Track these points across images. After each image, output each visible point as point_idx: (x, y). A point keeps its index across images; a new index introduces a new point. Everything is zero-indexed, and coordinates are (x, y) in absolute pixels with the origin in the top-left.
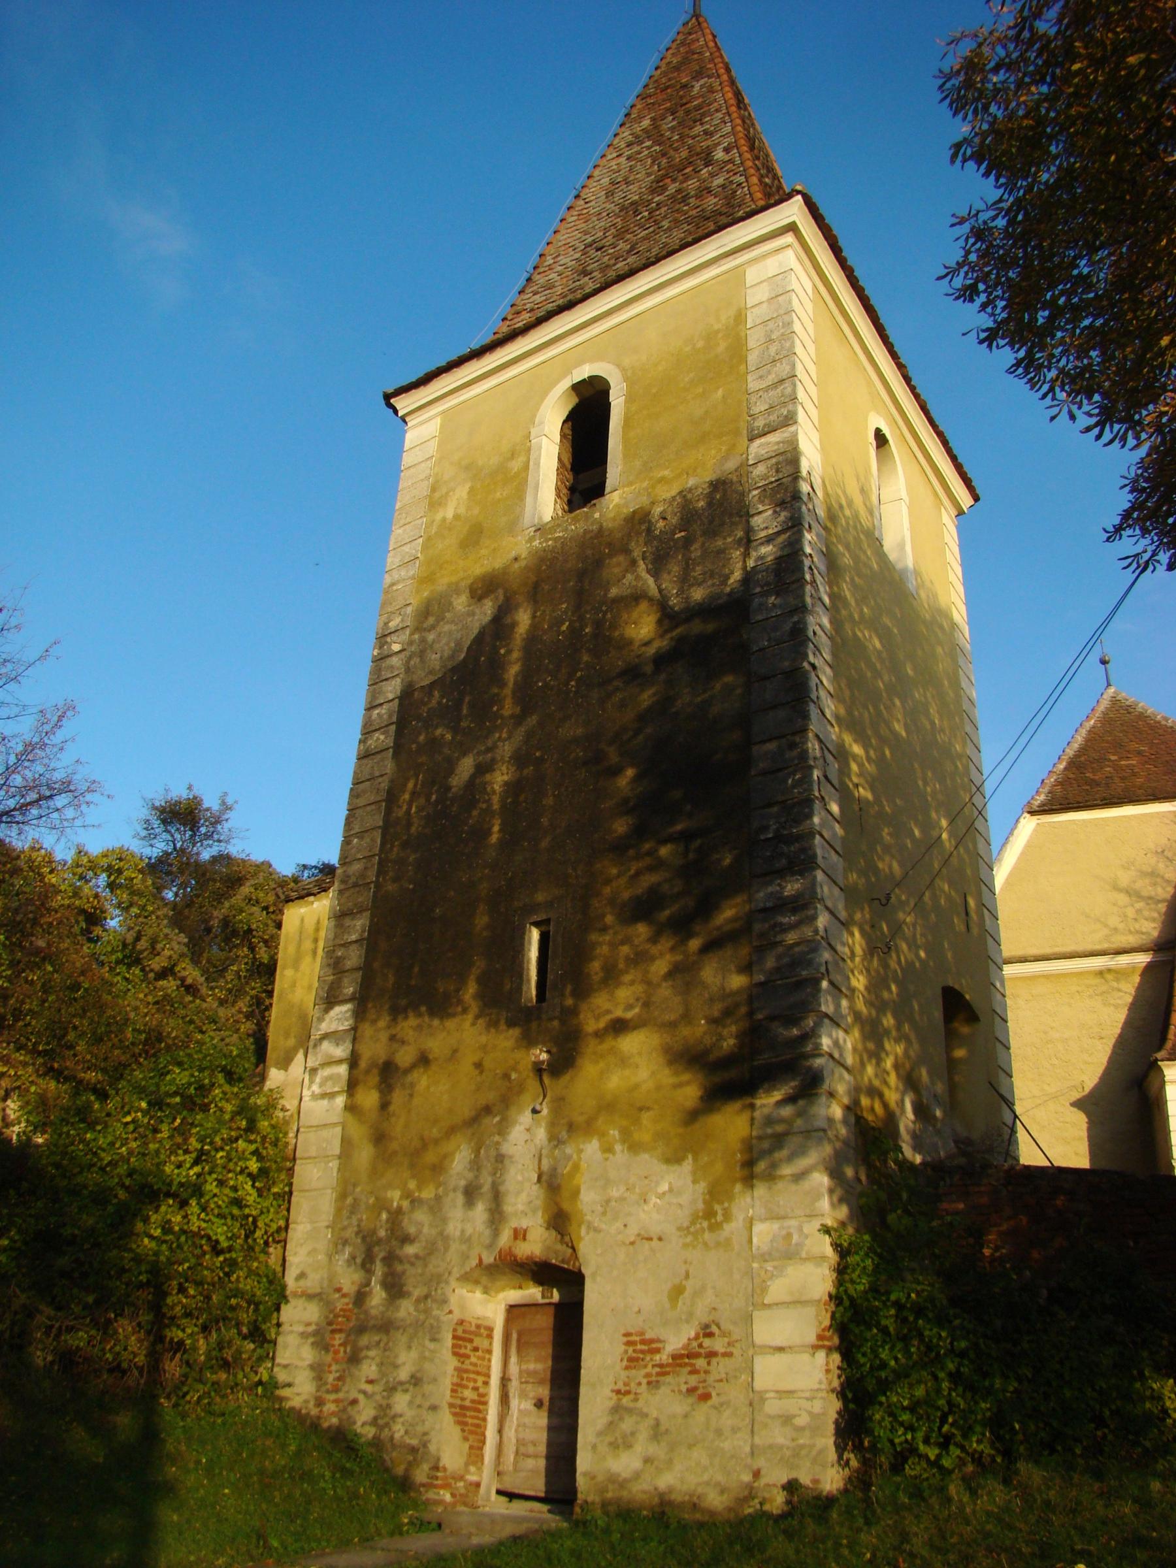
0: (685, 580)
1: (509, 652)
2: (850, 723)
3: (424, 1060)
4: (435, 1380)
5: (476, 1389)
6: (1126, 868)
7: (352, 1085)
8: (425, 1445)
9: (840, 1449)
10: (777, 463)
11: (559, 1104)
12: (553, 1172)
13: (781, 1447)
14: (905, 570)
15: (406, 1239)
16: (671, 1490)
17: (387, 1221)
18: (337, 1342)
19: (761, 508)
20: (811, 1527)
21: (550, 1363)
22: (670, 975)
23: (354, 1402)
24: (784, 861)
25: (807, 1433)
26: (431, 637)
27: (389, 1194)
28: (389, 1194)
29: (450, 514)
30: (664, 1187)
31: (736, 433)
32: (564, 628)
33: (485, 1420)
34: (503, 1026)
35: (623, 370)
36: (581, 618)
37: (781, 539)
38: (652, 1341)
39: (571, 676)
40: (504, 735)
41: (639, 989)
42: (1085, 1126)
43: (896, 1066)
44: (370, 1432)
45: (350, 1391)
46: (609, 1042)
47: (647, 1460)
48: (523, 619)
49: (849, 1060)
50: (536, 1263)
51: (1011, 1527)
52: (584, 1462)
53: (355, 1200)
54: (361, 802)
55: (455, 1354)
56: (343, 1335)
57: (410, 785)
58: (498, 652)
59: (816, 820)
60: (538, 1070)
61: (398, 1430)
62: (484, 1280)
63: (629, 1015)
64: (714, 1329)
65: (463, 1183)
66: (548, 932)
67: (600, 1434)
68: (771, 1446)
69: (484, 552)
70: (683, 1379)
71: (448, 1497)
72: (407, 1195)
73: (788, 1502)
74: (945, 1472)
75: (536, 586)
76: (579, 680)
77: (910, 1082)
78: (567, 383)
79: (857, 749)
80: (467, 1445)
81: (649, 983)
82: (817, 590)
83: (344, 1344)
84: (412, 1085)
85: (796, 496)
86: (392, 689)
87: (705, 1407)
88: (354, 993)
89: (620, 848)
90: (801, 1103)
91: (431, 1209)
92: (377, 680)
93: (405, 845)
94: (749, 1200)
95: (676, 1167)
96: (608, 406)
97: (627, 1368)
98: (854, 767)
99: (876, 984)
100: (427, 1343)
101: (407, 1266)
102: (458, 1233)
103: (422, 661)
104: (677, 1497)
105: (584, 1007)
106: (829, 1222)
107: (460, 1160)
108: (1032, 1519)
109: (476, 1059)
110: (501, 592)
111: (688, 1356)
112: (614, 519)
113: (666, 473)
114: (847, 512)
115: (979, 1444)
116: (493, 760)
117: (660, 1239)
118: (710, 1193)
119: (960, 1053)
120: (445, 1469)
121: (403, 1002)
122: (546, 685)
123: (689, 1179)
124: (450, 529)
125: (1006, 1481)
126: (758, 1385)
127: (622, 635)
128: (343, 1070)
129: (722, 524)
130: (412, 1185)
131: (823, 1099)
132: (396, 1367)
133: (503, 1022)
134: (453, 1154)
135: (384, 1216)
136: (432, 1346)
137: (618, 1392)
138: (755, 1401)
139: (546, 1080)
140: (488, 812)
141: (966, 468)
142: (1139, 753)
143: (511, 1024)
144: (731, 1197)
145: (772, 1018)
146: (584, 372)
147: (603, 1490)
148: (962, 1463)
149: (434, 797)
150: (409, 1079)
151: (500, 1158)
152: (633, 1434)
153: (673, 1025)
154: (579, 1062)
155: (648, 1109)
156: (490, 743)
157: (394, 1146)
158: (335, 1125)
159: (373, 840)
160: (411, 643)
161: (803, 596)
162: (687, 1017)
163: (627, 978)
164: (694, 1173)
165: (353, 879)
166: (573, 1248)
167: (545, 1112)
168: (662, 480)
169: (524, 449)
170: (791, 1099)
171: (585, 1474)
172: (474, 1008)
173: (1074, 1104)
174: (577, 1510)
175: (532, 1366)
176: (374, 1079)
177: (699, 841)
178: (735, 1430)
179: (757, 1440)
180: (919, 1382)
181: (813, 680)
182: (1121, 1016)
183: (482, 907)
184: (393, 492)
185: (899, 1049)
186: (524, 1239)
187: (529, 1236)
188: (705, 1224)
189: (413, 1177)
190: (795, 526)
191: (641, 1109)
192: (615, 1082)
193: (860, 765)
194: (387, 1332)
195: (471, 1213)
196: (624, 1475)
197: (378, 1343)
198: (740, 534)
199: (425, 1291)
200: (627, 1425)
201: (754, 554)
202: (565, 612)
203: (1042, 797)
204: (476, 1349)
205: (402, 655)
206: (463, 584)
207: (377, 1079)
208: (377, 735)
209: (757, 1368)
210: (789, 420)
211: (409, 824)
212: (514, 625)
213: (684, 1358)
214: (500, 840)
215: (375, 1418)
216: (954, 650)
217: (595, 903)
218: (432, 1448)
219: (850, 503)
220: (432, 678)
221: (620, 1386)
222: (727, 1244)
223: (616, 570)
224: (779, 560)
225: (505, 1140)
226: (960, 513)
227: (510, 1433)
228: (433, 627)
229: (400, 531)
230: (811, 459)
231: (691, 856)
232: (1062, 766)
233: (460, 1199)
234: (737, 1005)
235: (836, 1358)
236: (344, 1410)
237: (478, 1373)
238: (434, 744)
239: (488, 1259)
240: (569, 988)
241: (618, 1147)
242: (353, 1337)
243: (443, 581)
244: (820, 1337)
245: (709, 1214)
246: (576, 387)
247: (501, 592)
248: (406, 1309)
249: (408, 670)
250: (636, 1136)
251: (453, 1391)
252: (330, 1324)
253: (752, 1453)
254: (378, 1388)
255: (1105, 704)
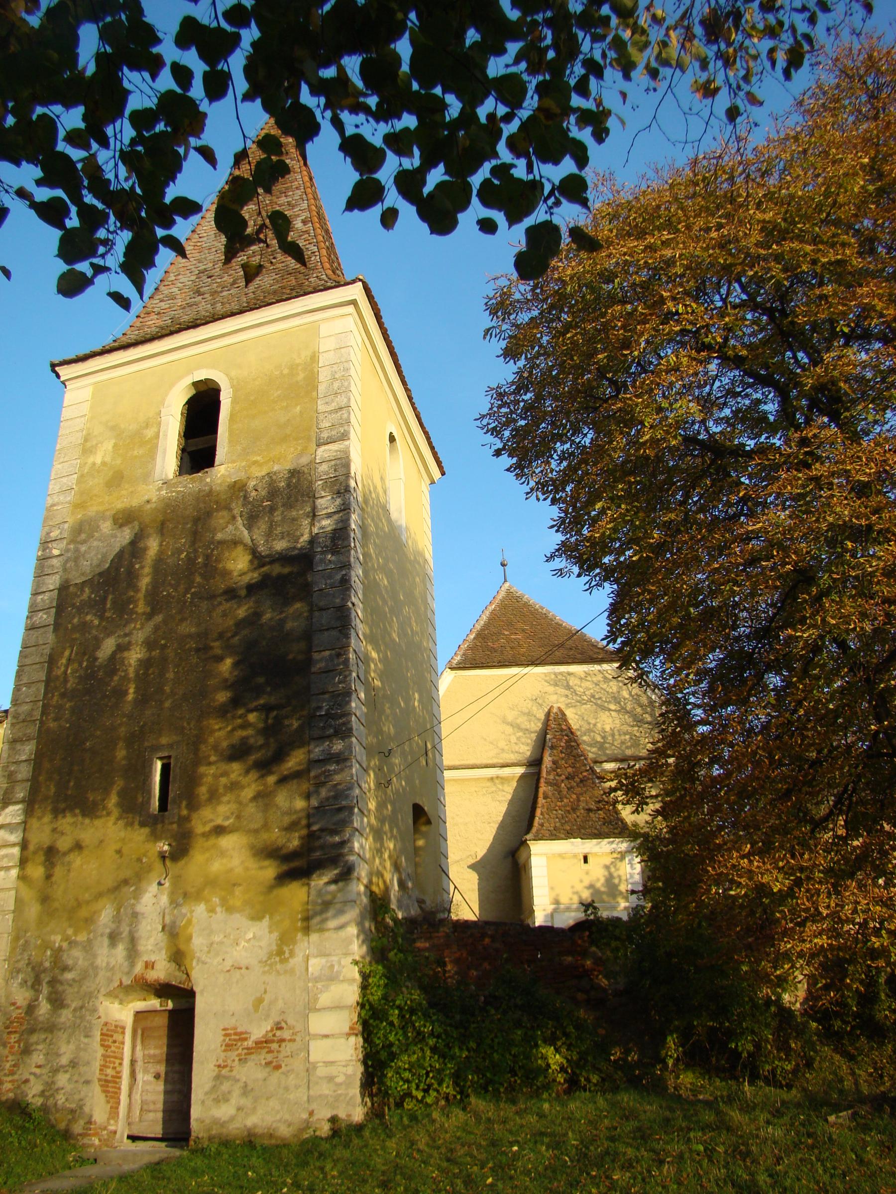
0: (269, 534)
1: (142, 567)
2: (372, 639)
3: (78, 846)
4: (88, 1063)
5: (114, 1068)
6: (512, 709)
7: (23, 862)
8: (81, 1107)
9: (363, 1095)
10: (336, 465)
11: (177, 880)
12: (174, 923)
13: (327, 1096)
14: (400, 527)
15: (65, 969)
16: (255, 1126)
17: (51, 956)
18: (12, 1040)
19: (323, 494)
20: (356, 1141)
21: (165, 1049)
22: (255, 798)
23: (27, 1081)
24: (332, 731)
25: (343, 1087)
26: (83, 548)
27: (53, 938)
28: (53, 938)
29: (99, 461)
30: (250, 935)
31: (309, 439)
32: (183, 556)
33: (120, 1088)
34: (137, 826)
35: (231, 379)
36: (196, 551)
37: (336, 517)
38: (242, 1033)
39: (187, 591)
40: (138, 626)
41: (234, 806)
42: (476, 881)
43: (390, 857)
44: (39, 1101)
45: (23, 1073)
46: (212, 841)
47: (239, 1109)
48: (153, 545)
49: (368, 856)
50: (160, 984)
51: (470, 1133)
52: (196, 1112)
53: (26, 942)
54: (28, 661)
55: (102, 1045)
56: (17, 1035)
57: (67, 653)
58: (133, 566)
59: (353, 705)
60: (163, 857)
61: (61, 1099)
62: (121, 995)
63: (226, 823)
64: (283, 1024)
65: (108, 931)
66: (169, 764)
67: (206, 1094)
68: (320, 1096)
69: (124, 492)
70: (263, 1057)
71: (97, 1142)
72: (66, 938)
73: (332, 1129)
74: (428, 1105)
75: (163, 523)
76: (193, 594)
77: (397, 867)
78: (189, 380)
79: (374, 655)
80: (109, 1106)
81: (240, 803)
82: (356, 552)
83: (18, 1042)
84: (69, 863)
85: (347, 490)
86: (53, 582)
87: (277, 1074)
88: (24, 798)
89: (223, 712)
90: (341, 884)
91: (84, 947)
92: (40, 574)
93: (63, 695)
94: (306, 944)
95: (258, 923)
96: (218, 403)
97: (225, 1051)
98: (372, 666)
99: (381, 806)
100: (82, 1039)
101: (66, 987)
102: (104, 965)
103: (77, 565)
104: (259, 1131)
105: (195, 816)
106: (357, 958)
107: (106, 915)
108: (482, 1127)
109: (117, 846)
110: (136, 523)
111: (266, 1042)
112: (221, 485)
113: (259, 458)
114: (374, 496)
115: (447, 1088)
116: (130, 643)
117: (247, 968)
118: (281, 939)
119: (421, 843)
120: (95, 1123)
121: (62, 806)
122: (169, 595)
123: (267, 930)
124: (98, 472)
125: (464, 1109)
126: (312, 1058)
127: (224, 567)
128: (16, 851)
129: (297, 501)
130: (70, 932)
131: (355, 881)
132: (58, 1055)
133: (136, 823)
134: (101, 911)
135: (49, 953)
136: (86, 1040)
137: (219, 1066)
138: (310, 1069)
139: (168, 862)
140: (125, 678)
141: (439, 455)
142: (523, 630)
143: (142, 824)
144: (294, 942)
145: (322, 830)
146: (201, 375)
147: (209, 1129)
148: (437, 1101)
149: (85, 664)
150: (67, 859)
151: (135, 915)
152: (229, 1092)
153: (256, 831)
154: (191, 852)
155: (240, 885)
156: (127, 630)
157: (56, 905)
158: (9, 889)
159: (38, 689)
160: (67, 550)
161: (349, 557)
162: (266, 826)
163: (225, 799)
164: (270, 927)
165: (22, 717)
166: (187, 974)
167: (167, 885)
168: (255, 463)
169: (155, 421)
170: (335, 881)
171: (197, 1120)
172: (116, 812)
173: (469, 867)
174: (192, 1143)
175: (152, 1052)
176: (41, 858)
177: (275, 713)
178: (297, 1087)
179: (312, 1093)
180: (414, 1053)
181: (353, 614)
182: (503, 808)
183: (121, 744)
184: (55, 437)
185: (391, 846)
186: (153, 968)
187: (157, 966)
188: (278, 959)
189: (70, 926)
190: (345, 509)
191: (234, 885)
192: (216, 866)
193: (376, 665)
194: (51, 1032)
195: (113, 951)
196: (223, 1119)
197: (45, 1040)
198: (308, 509)
199: (80, 1003)
200: (226, 1086)
201: (317, 525)
202: (184, 545)
203: (459, 658)
204: (115, 1042)
205: (61, 559)
206: (108, 513)
207: (43, 858)
208: (41, 614)
209: (311, 1048)
210: (344, 437)
211: (66, 681)
212: (146, 549)
213: (263, 1044)
214: (135, 700)
215: (43, 1092)
216: (426, 577)
217: (203, 747)
218: (87, 1109)
219: (375, 488)
220: (84, 579)
221: (220, 1062)
222: (292, 971)
223: (221, 521)
224: (335, 530)
225: (138, 902)
226: (433, 482)
227: (137, 1097)
228: (84, 542)
229: (59, 466)
230: (356, 467)
231: (270, 721)
232: (472, 637)
233: (106, 941)
234: (300, 819)
235: (360, 1039)
236: (19, 1087)
237: (116, 1058)
238: (84, 627)
239: (127, 981)
240: (184, 803)
241: (219, 909)
242: (25, 1036)
243: (93, 510)
244: (351, 1028)
245: (280, 953)
246: (195, 384)
247: (136, 523)
248: (66, 1015)
249: (65, 570)
250: (231, 902)
251: (101, 1070)
252: (7, 1028)
253: (308, 1101)
254: (44, 1071)
255: (503, 594)
